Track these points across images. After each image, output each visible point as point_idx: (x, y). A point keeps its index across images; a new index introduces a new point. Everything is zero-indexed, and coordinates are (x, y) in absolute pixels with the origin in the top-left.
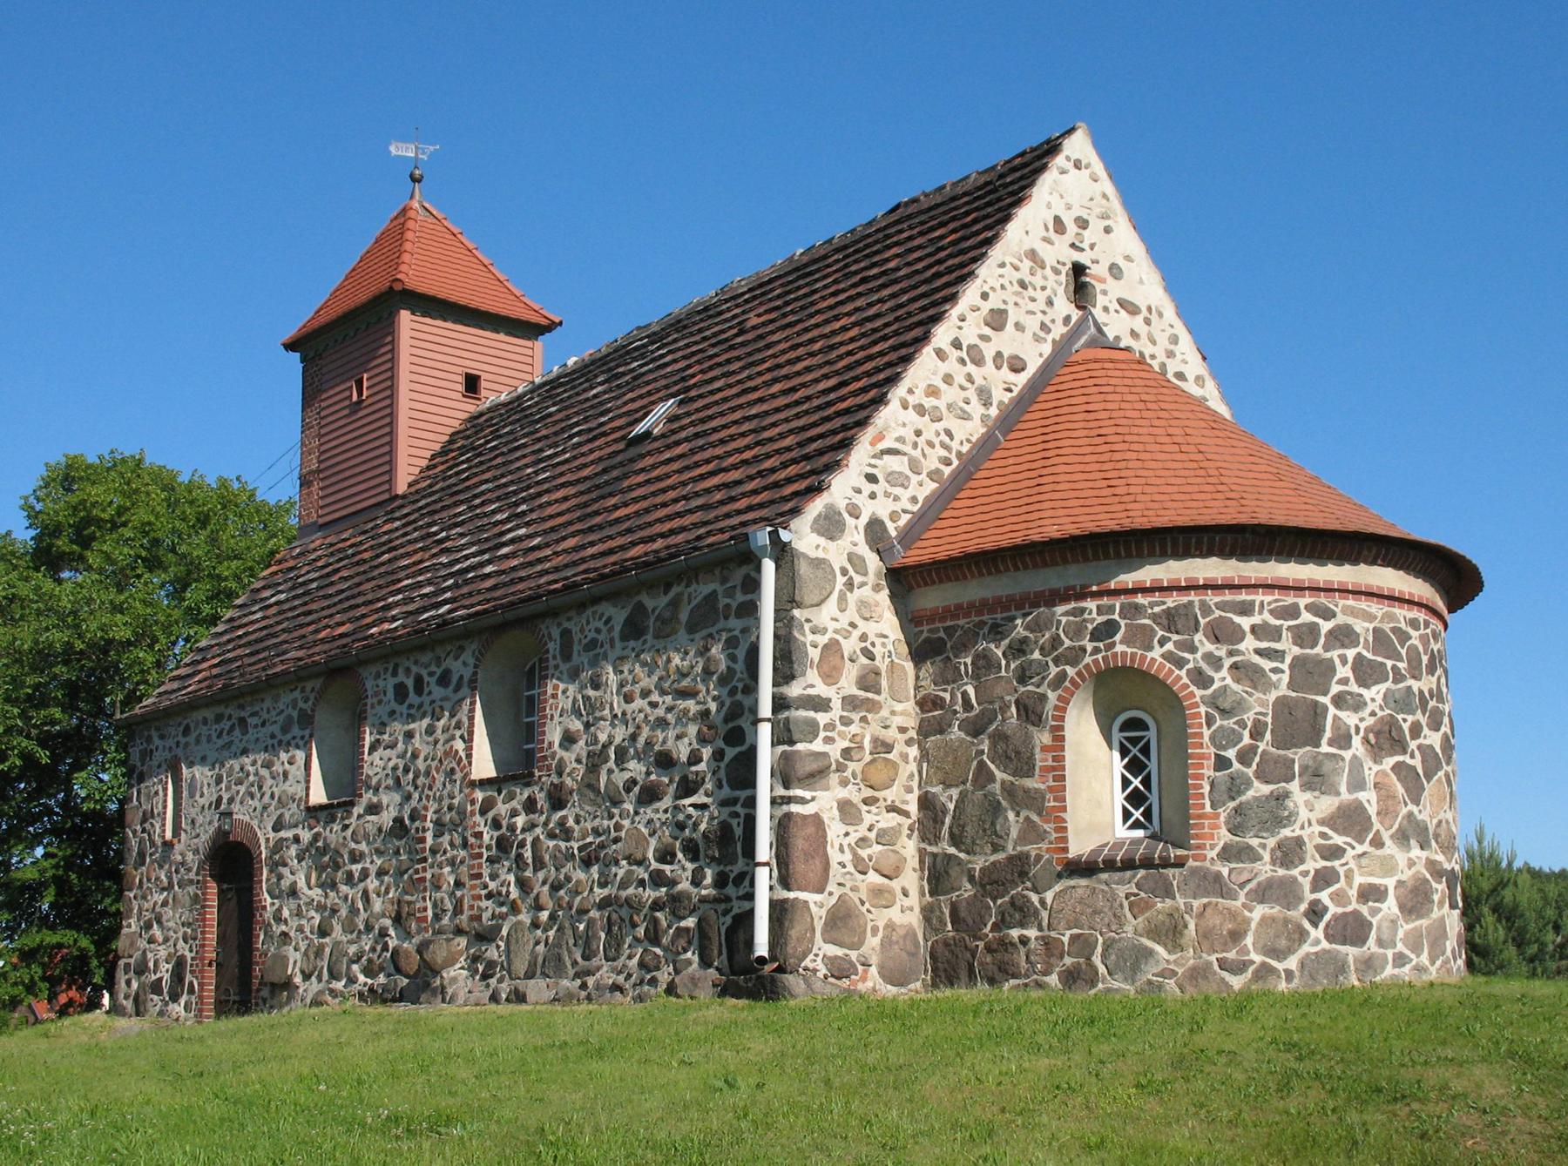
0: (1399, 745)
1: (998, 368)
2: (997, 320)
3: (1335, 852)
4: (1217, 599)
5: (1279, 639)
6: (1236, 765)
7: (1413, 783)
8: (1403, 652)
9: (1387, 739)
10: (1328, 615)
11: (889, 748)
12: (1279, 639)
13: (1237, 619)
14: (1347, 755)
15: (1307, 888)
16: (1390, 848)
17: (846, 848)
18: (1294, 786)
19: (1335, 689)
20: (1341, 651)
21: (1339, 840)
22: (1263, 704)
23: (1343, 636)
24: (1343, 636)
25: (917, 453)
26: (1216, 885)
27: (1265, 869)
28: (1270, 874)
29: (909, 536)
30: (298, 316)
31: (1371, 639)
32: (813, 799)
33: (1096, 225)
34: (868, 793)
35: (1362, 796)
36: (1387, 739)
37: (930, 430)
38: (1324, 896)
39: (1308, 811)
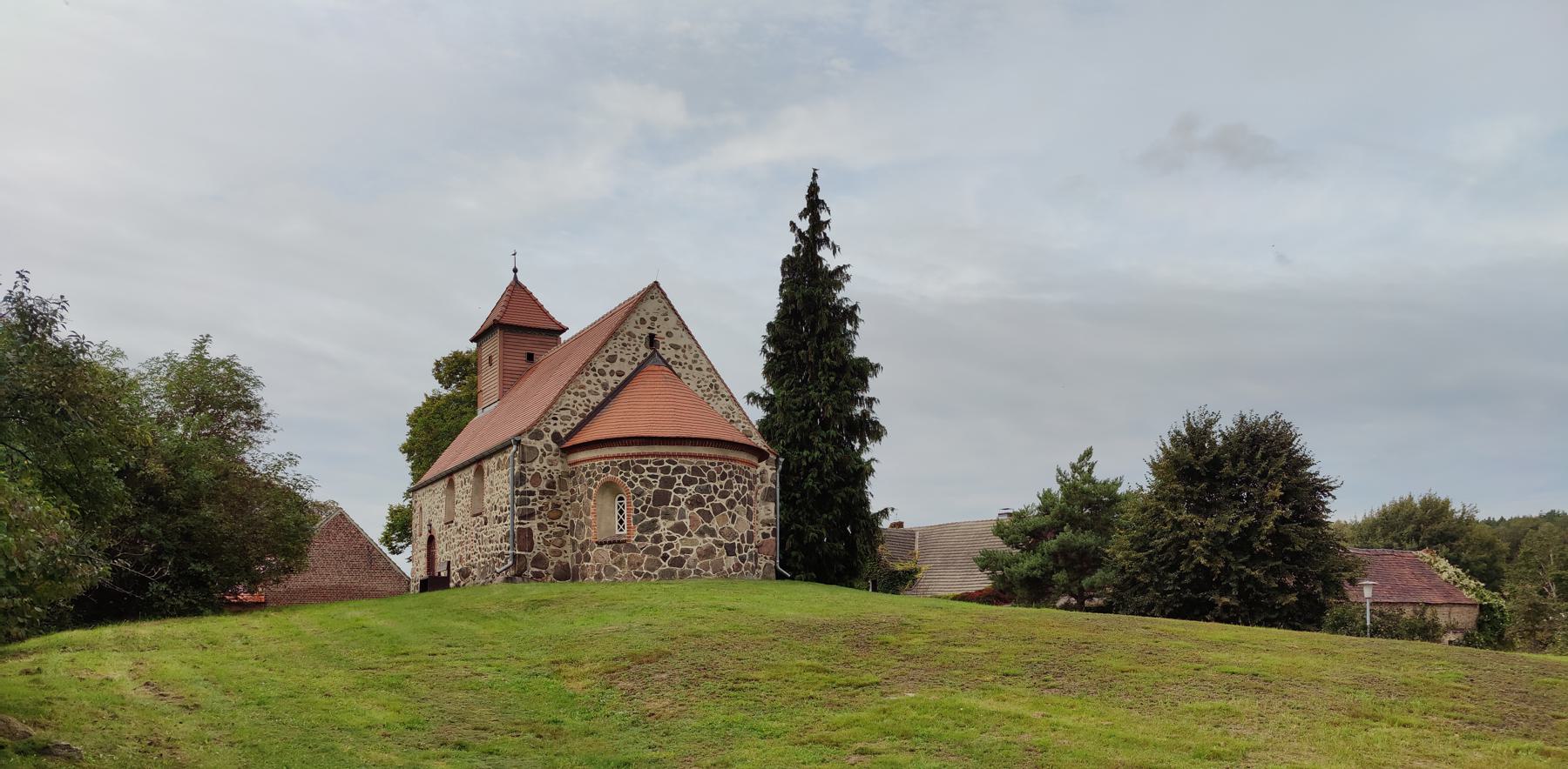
0: (701, 503)
2: (612, 359)
7: (707, 517)
9: (695, 502)
16: (695, 536)
23: (681, 470)
24: (680, 470)
26: (634, 549)
27: (649, 544)
29: (569, 437)
30: (473, 334)
33: (660, 319)
36: (695, 502)
39: (664, 527)
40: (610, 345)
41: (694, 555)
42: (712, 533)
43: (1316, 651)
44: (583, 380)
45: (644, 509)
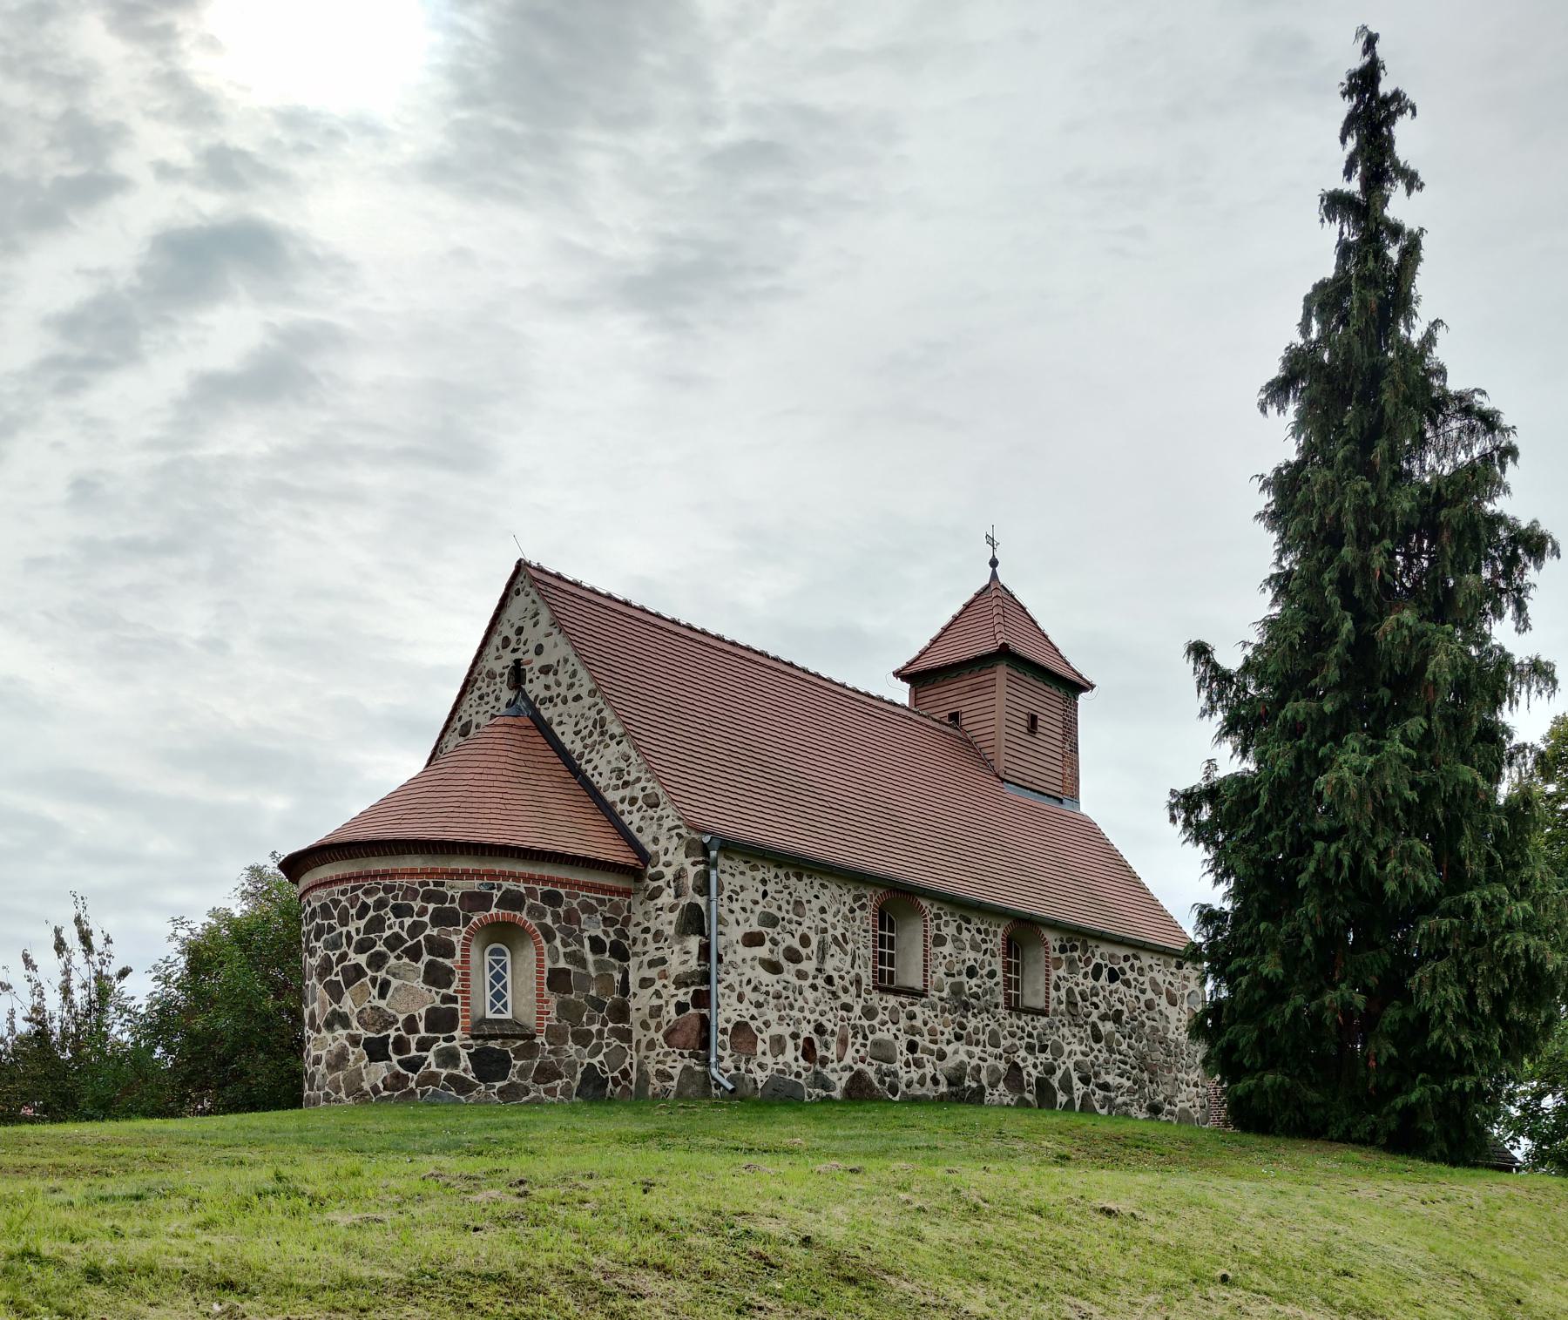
8: (336, 913)
42: (344, 1021)
43: (404, 1118)
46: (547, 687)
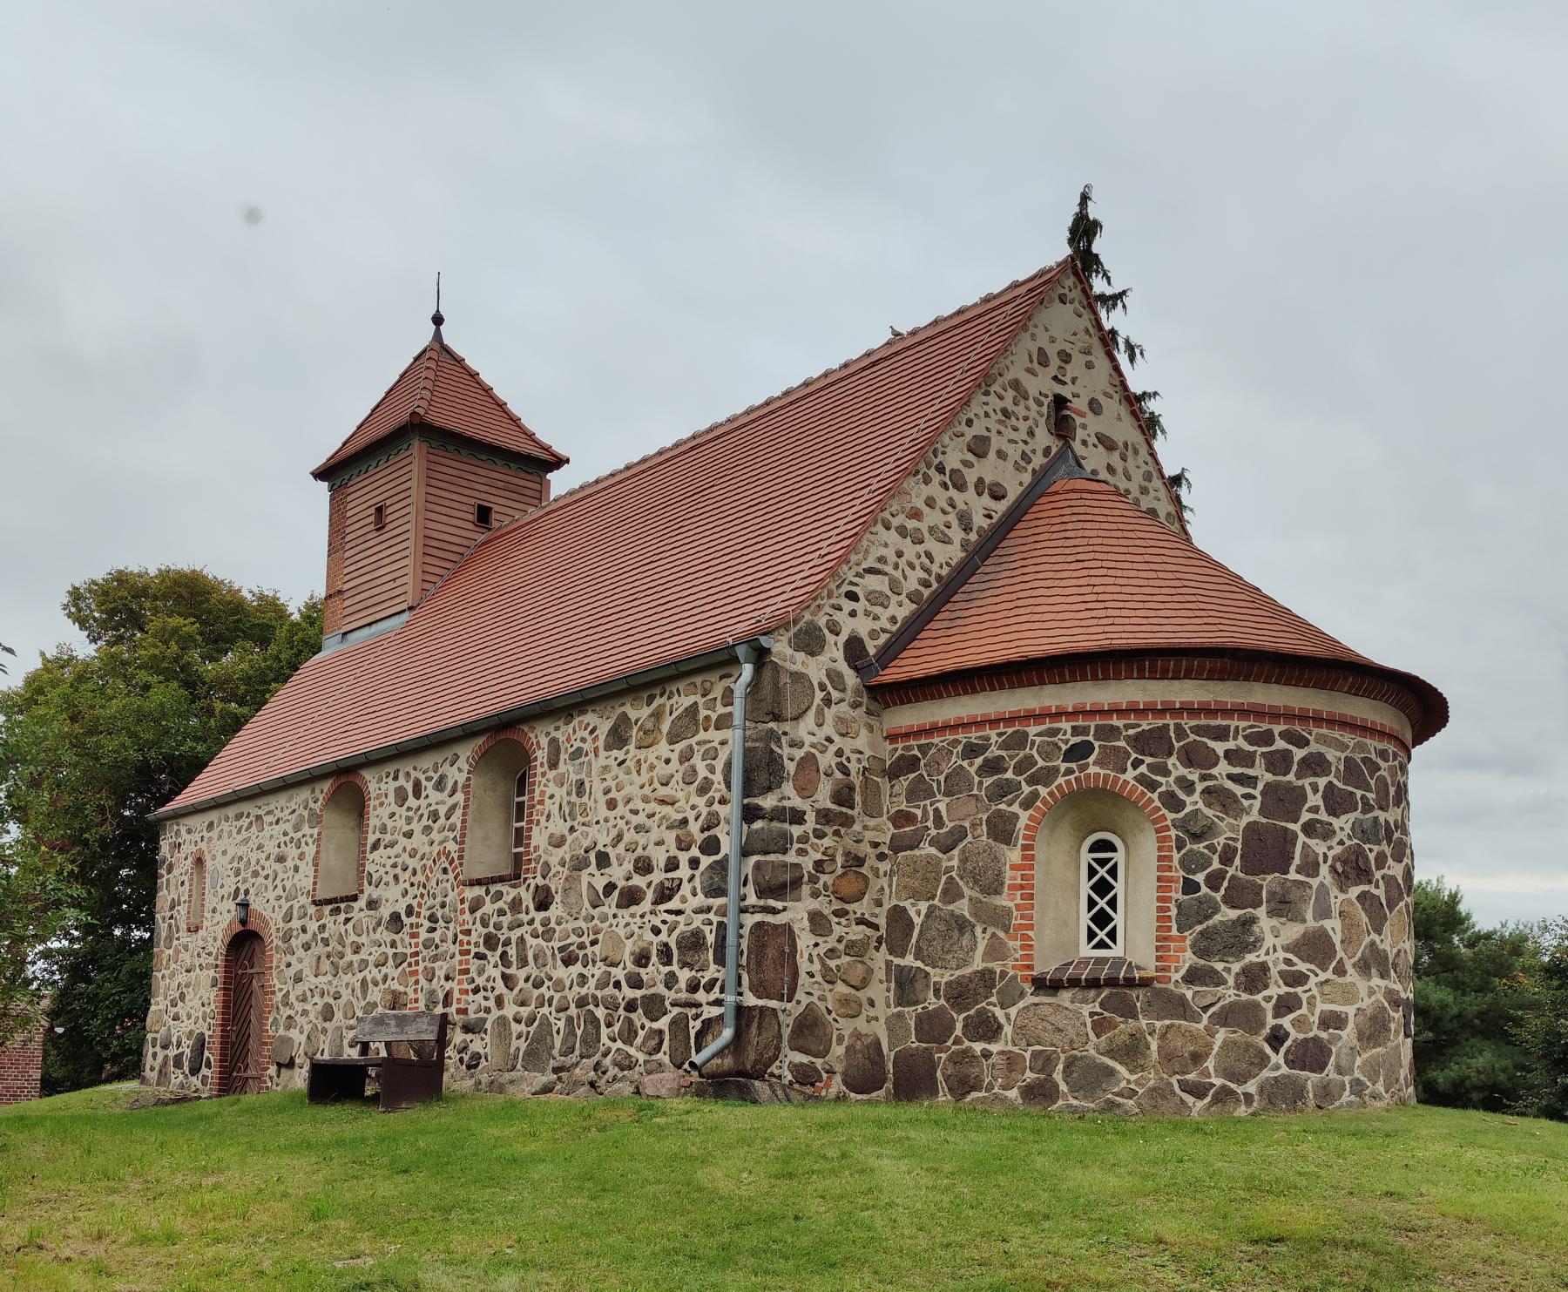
0: (1364, 874)
1: (980, 494)
2: (979, 448)
3: (1297, 979)
4: (1193, 723)
5: (1252, 766)
6: (1205, 890)
10: (1302, 742)
11: (860, 862)
12: (1252, 766)
13: (1211, 744)
14: (1315, 882)
15: (1269, 1014)
16: (1352, 976)
17: (815, 959)
18: (1261, 912)
19: (1306, 816)
20: (1312, 779)
21: (1302, 967)
22: (1233, 829)
23: (1316, 765)
25: (898, 574)
26: (1180, 1008)
27: (1229, 994)
28: (1233, 998)
29: (891, 652)
30: (320, 459)
31: (1342, 768)
32: (785, 909)
34: (837, 905)
35: (1327, 924)
37: (910, 551)
38: (1286, 1022)
39: (1274, 939)
40: (976, 408)
41: (1348, 1034)
44: (918, 493)
45: (1214, 881)
46: (1111, 469)
